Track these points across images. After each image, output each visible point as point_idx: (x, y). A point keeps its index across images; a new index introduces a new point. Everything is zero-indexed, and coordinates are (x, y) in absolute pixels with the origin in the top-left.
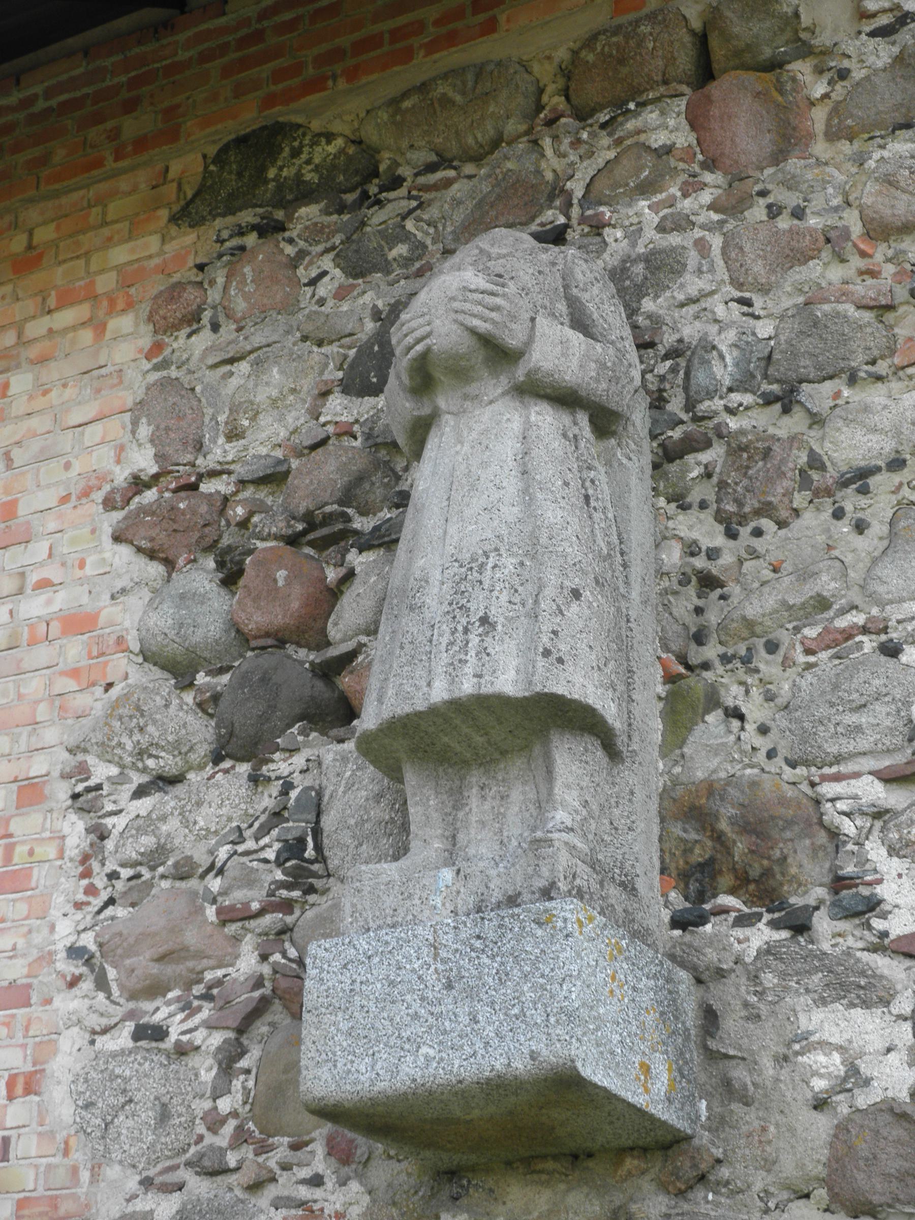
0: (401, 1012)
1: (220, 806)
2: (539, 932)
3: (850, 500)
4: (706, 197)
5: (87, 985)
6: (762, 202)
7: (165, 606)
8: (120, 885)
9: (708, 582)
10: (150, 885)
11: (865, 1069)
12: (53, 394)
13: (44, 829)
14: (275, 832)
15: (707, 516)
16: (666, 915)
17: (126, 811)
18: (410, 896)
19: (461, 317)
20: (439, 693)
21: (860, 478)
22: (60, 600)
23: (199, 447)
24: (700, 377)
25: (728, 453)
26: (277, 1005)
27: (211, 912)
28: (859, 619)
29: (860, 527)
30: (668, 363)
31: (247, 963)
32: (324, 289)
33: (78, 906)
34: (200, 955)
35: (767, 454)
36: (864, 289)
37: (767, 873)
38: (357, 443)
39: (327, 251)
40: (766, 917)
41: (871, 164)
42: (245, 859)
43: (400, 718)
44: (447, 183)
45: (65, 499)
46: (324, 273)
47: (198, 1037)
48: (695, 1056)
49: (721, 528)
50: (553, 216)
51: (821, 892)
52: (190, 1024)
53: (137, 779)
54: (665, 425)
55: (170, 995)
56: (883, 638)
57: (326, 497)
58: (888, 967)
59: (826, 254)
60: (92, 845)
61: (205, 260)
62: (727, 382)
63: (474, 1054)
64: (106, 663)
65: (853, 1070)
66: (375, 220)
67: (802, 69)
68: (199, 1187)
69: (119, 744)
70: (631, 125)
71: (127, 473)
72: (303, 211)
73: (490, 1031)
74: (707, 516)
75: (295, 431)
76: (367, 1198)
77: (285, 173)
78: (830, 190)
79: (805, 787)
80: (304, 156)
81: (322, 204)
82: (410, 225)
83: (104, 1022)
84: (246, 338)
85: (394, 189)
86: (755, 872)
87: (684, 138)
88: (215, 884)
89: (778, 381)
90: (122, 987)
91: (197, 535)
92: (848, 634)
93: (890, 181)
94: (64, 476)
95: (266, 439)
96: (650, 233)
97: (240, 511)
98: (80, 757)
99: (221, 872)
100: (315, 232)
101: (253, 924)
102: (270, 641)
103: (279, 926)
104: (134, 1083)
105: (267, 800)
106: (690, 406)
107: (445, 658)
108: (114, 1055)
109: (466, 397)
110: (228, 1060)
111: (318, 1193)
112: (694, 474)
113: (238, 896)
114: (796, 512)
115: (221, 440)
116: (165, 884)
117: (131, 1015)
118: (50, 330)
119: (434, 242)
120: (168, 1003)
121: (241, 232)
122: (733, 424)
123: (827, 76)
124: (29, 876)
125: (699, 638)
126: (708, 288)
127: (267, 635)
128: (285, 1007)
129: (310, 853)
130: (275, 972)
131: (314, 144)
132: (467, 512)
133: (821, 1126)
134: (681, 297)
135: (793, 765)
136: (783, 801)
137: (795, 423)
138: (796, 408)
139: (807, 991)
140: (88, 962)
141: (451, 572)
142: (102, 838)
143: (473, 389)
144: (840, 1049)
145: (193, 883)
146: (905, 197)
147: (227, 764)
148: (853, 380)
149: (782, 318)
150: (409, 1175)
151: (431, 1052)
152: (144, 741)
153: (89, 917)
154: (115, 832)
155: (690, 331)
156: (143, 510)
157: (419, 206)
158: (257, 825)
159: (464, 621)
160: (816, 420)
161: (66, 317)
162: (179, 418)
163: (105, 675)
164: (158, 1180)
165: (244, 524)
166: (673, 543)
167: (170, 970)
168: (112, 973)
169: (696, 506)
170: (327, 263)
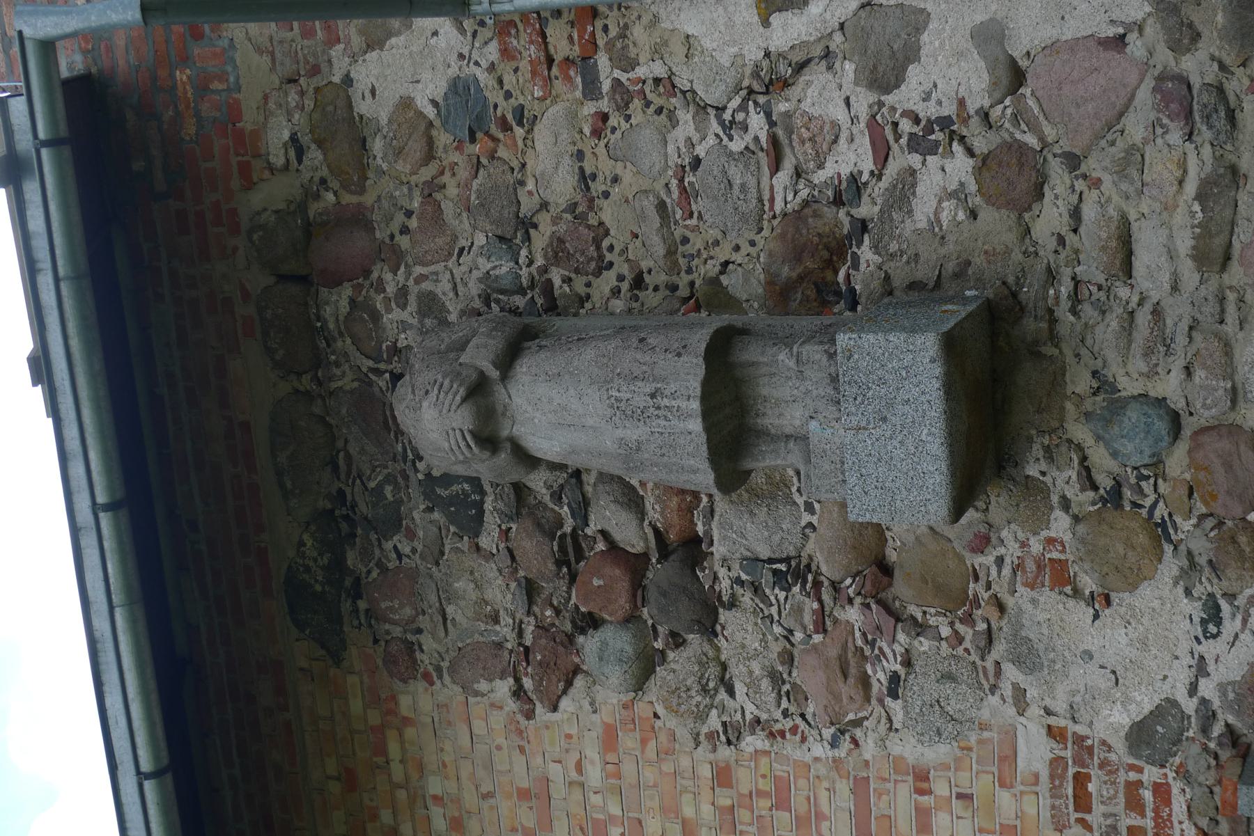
0: (899, 453)
1: (747, 631)
2: (856, 356)
3: (597, 187)
4: (388, 276)
5: (858, 733)
6: (398, 238)
7: (606, 671)
8: (792, 709)
9: (638, 282)
10: (794, 685)
11: (953, 187)
12: (446, 759)
13: (749, 767)
14: (767, 591)
15: (596, 282)
16: (848, 313)
17: (745, 703)
18: (824, 451)
19: (454, 407)
20: (696, 425)
21: (585, 179)
22: (592, 753)
23: (499, 645)
24: (506, 283)
25: (558, 266)
26: (882, 595)
27: (818, 638)
28: (674, 182)
29: (616, 180)
30: (493, 305)
31: (853, 614)
32: (406, 549)
33: (804, 739)
34: (845, 648)
35: (561, 241)
36: (463, 173)
37: (827, 247)
38: (514, 527)
39: (380, 545)
40: (855, 249)
41: (385, 166)
42: (783, 615)
43: (710, 454)
44: (348, 457)
45: (522, 750)
46: (395, 547)
47: (899, 649)
48: (936, 295)
49: (605, 273)
50: (382, 382)
51: (842, 214)
52: (890, 656)
53: (723, 695)
54: (530, 322)
55: (870, 672)
56: (688, 168)
57: (547, 549)
58: (892, 169)
59: (438, 196)
60: (763, 730)
61: (371, 639)
62: (512, 264)
63: (929, 402)
64: (640, 718)
65: (952, 195)
66: (365, 510)
67: (314, 208)
68: (1000, 649)
69: (697, 706)
70: (331, 326)
71: (510, 701)
72: (349, 562)
73: (915, 392)
74: (596, 282)
75: (500, 571)
76: (1012, 526)
77: (320, 578)
78: (397, 193)
79: (775, 222)
80: (311, 564)
81: (347, 548)
82: (372, 485)
83: (884, 720)
84: (431, 607)
85: (345, 496)
86: (826, 254)
87: (347, 291)
88: (799, 636)
89: (515, 232)
90: (861, 709)
91: (561, 649)
92: (683, 190)
93: (399, 152)
94: (505, 751)
95: (501, 593)
96: (404, 315)
97: (548, 613)
98: (702, 738)
99: (791, 632)
100: (366, 554)
101: (827, 609)
102: (639, 592)
103: (830, 589)
104: (927, 698)
105: (747, 598)
106: (522, 291)
107: (674, 422)
108: (907, 713)
109: (504, 414)
110: (920, 628)
111: (1008, 560)
112: (567, 289)
113: (808, 619)
114: (601, 224)
115: (497, 628)
116: (794, 674)
117: (881, 701)
118: (401, 761)
119: (386, 467)
120: (875, 672)
121: (356, 611)
122: (540, 262)
123: (322, 192)
124: (780, 778)
125: (674, 288)
126: (448, 276)
127: (634, 596)
128: (884, 590)
129: (783, 567)
130: (859, 594)
131: (303, 556)
132: (581, 411)
133: (988, 215)
134: (451, 295)
135: (761, 230)
136: (783, 236)
137: (544, 220)
138: (535, 220)
139: (903, 222)
140: (843, 732)
141: (618, 421)
142: (758, 721)
143: (500, 409)
144: (940, 202)
145: (796, 653)
146: (410, 143)
147: (718, 628)
148: (522, 183)
149: (475, 228)
150: (998, 496)
151: (925, 432)
152: (696, 687)
153: (813, 732)
154: (756, 712)
155: (474, 289)
156: (537, 689)
157: (360, 477)
158: (761, 605)
159: (652, 410)
160: (544, 206)
161: (394, 749)
162: (478, 659)
163: (648, 719)
164: (992, 681)
165: (558, 612)
166: (610, 304)
167: (853, 671)
168: (851, 716)
169: (588, 290)
170: (388, 545)
